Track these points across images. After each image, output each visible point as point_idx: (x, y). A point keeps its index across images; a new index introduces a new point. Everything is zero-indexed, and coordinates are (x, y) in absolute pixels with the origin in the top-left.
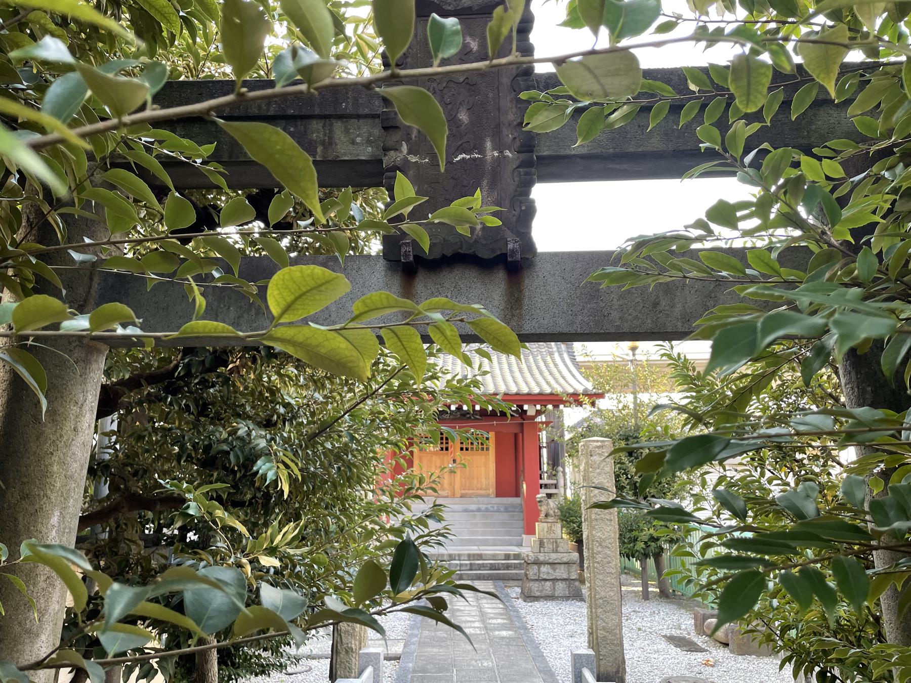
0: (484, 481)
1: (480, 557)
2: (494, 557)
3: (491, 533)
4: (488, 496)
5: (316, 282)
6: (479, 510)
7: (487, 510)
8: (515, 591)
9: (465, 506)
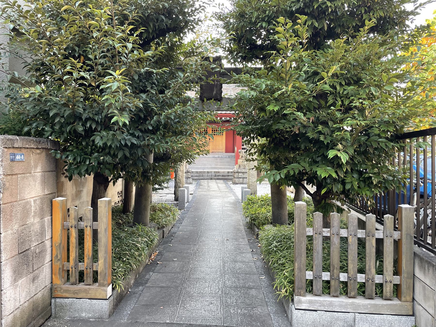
0: (221, 147)
1: (219, 172)
2: (224, 172)
3: (223, 165)
4: (222, 152)
5: (208, 183)
6: (219, 157)
7: (222, 157)
8: (230, 183)
9: (213, 156)
